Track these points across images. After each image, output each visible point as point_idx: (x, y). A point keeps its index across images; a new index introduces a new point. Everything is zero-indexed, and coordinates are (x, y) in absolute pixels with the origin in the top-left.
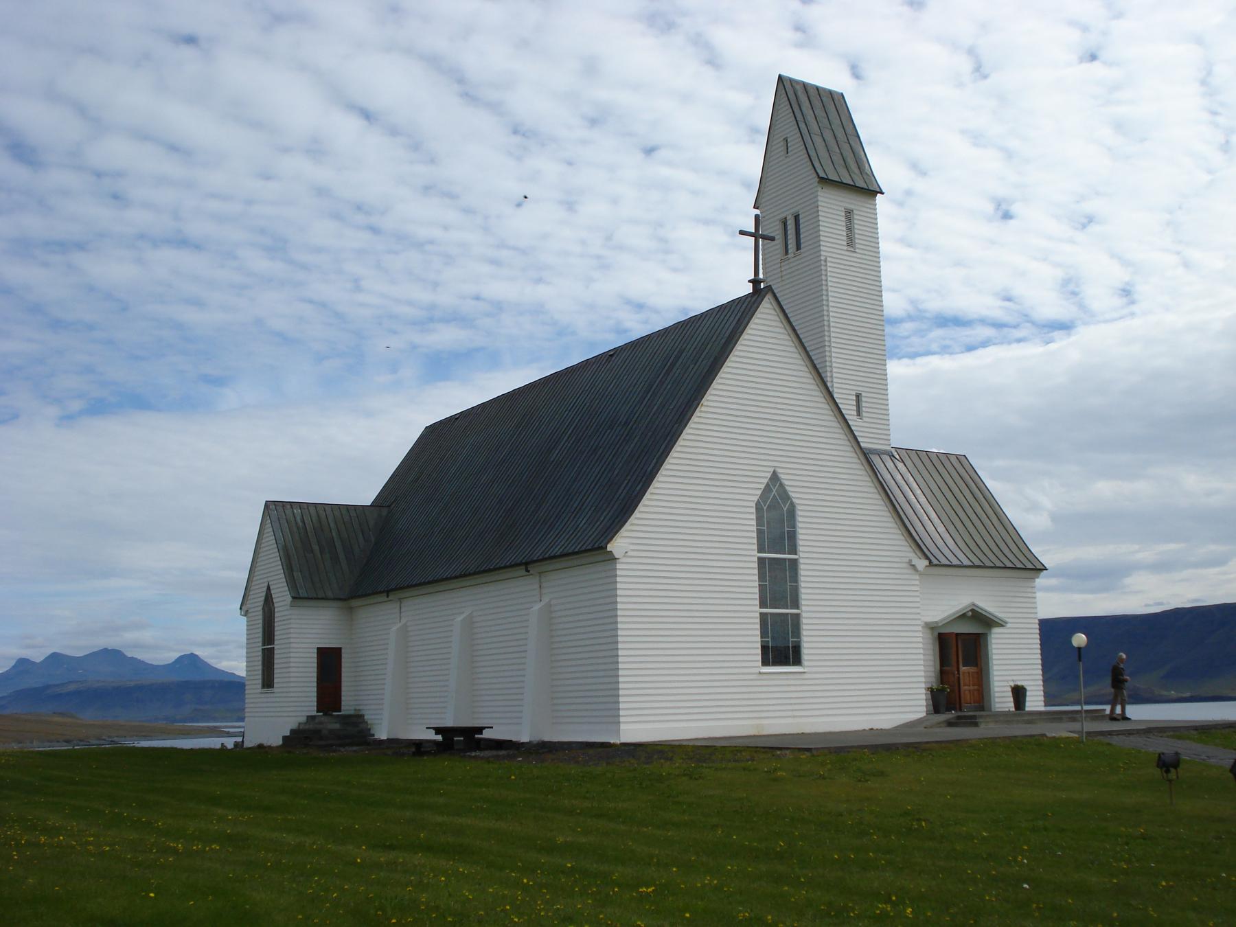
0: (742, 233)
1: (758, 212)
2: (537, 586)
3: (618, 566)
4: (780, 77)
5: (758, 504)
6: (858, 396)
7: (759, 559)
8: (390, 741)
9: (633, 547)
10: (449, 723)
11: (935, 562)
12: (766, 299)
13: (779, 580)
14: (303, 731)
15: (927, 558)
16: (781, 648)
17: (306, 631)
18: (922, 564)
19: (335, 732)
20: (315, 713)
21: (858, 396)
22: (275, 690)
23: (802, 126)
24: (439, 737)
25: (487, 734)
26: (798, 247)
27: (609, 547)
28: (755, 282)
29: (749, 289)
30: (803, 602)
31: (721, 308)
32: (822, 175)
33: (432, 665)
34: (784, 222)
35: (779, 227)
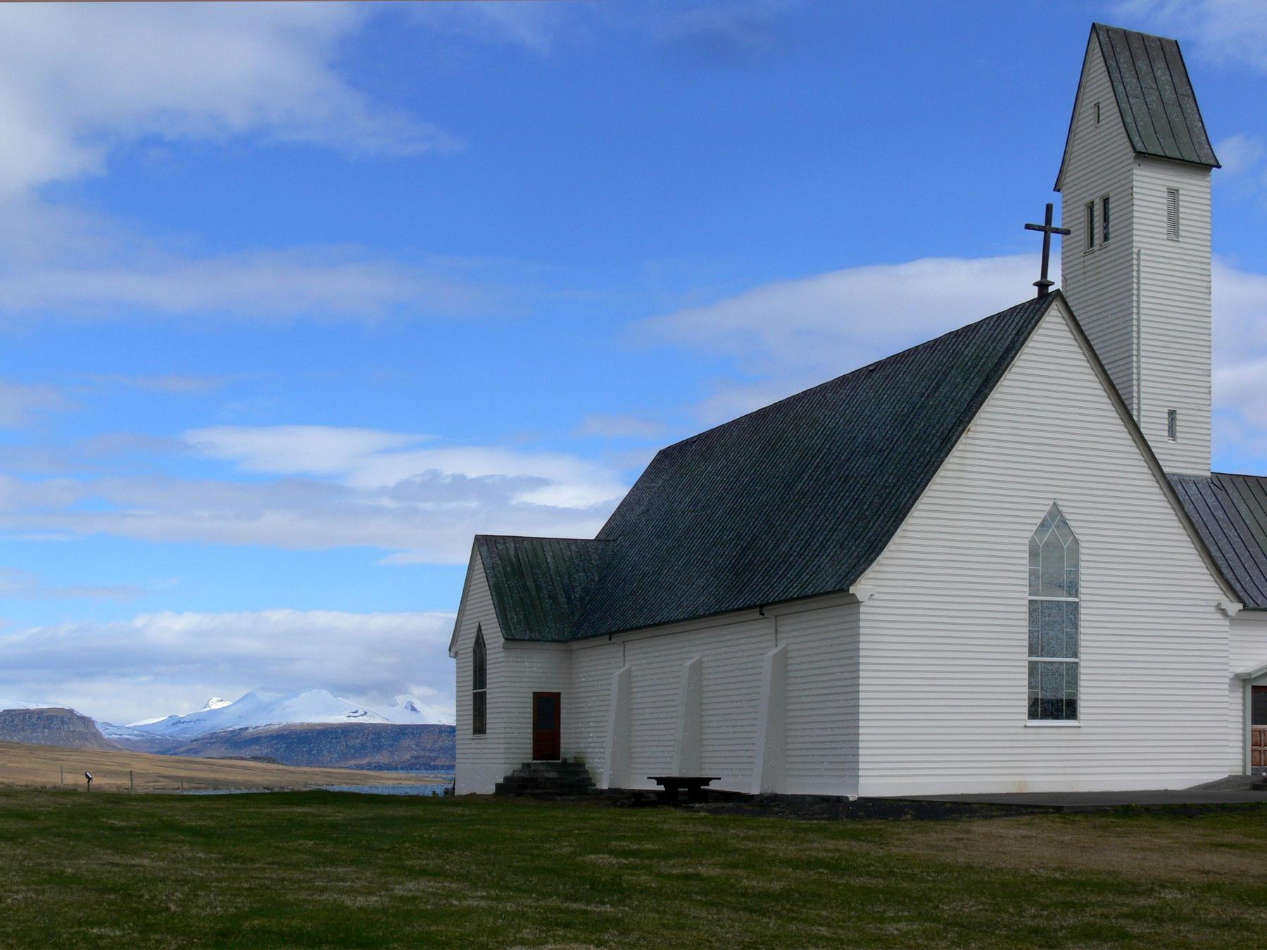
0: (1028, 227)
1: (1056, 199)
2: (773, 630)
3: (862, 610)
4: (1094, 25)
5: (1032, 541)
6: (1172, 413)
7: (1030, 601)
8: (612, 791)
9: (879, 589)
10: (675, 773)
11: (1251, 604)
12: (1054, 305)
13: (1053, 626)
14: (524, 779)
15: (1241, 600)
16: (1054, 704)
17: (518, 676)
18: (1234, 608)
19: (551, 776)
20: (530, 761)
21: (1172, 413)
22: (488, 736)
23: (1120, 88)
24: (662, 788)
25: (713, 786)
26: (1106, 238)
27: (852, 590)
28: (1043, 285)
29: (1033, 293)
30: (1082, 650)
31: (1000, 316)
32: (1140, 147)
33: (654, 711)
34: (1091, 207)
35: (1082, 214)
